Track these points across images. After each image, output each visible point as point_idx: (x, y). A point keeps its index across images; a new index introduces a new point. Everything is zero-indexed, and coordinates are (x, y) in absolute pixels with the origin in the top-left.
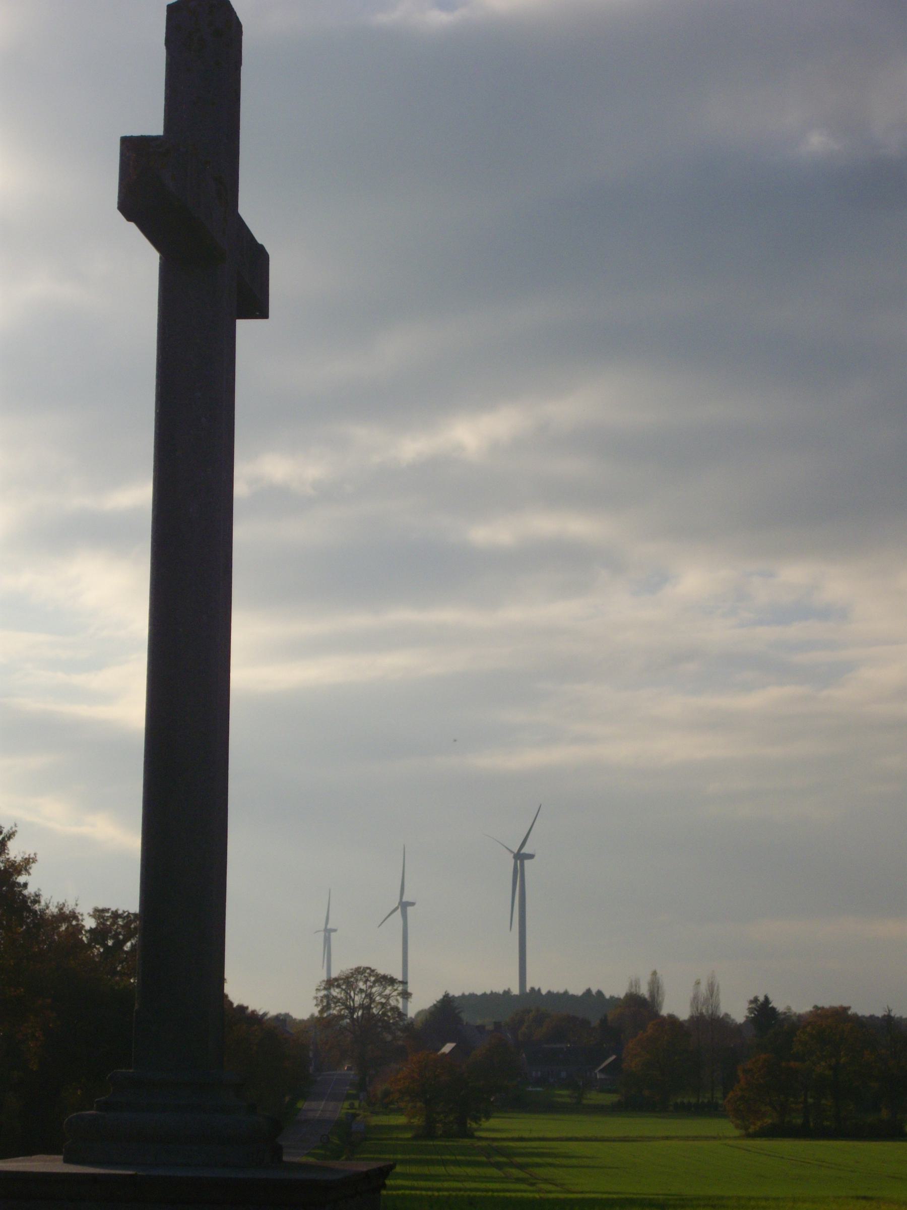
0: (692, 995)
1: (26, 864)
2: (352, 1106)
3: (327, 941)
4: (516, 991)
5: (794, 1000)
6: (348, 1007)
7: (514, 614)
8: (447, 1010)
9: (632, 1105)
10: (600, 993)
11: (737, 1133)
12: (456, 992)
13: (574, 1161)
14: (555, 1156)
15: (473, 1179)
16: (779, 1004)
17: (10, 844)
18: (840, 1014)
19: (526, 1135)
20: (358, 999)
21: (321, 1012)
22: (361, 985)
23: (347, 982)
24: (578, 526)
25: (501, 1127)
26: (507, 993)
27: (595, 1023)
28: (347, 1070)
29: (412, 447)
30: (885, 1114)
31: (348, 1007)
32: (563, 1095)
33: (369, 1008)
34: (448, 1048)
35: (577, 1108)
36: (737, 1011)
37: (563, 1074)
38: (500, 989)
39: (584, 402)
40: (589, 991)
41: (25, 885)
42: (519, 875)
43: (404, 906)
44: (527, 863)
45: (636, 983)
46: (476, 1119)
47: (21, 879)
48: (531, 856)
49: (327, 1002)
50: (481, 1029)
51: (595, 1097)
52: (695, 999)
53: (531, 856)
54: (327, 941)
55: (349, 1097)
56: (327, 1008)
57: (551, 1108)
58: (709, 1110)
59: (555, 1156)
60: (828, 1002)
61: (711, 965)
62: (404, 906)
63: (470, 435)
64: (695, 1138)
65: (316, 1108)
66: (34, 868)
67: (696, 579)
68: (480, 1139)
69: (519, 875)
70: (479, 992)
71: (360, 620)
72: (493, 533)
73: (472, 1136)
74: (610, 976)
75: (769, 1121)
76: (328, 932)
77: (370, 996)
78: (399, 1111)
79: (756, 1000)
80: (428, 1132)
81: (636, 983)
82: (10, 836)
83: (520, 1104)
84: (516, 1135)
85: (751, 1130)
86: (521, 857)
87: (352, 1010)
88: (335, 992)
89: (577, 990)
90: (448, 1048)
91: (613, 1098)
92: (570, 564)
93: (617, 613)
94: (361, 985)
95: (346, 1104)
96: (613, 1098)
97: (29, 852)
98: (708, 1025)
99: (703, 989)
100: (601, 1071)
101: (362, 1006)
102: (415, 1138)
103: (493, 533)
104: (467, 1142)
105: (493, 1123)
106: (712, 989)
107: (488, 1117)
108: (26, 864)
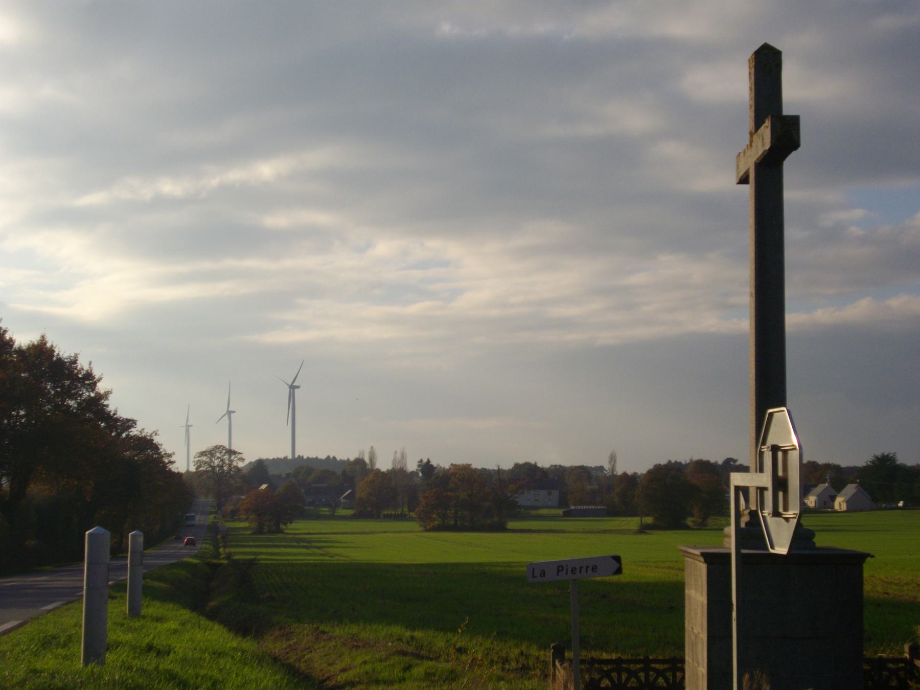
0: (392, 458)
1: (106, 395)
2: (215, 518)
3: (187, 431)
4: (290, 457)
5: (443, 461)
6: (211, 466)
7: (288, 263)
8: (260, 467)
9: (361, 515)
10: (334, 458)
11: (421, 529)
12: (264, 457)
13: (336, 545)
14: (337, 542)
15: (296, 555)
16: (434, 463)
17: (99, 385)
18: (467, 468)
19: (311, 531)
20: (216, 462)
21: (197, 468)
22: (218, 455)
23: (211, 453)
24: (321, 218)
25: (299, 527)
26: (285, 458)
27: (339, 472)
28: (211, 499)
29: (235, 175)
30: (496, 519)
31: (211, 466)
32: (325, 510)
33: (222, 467)
34: (264, 486)
35: (332, 517)
36: (412, 466)
37: (324, 500)
38: (282, 456)
39: (320, 156)
40: (329, 457)
41: (107, 406)
42: (292, 396)
43: (230, 413)
44: (296, 390)
45: (362, 453)
46: (285, 524)
47: (106, 403)
48: (298, 387)
49: (199, 464)
50: (279, 476)
51: (341, 512)
52: (394, 460)
53: (298, 387)
54: (187, 431)
55: (211, 513)
56: (200, 466)
57: (319, 517)
58: (401, 517)
59: (337, 542)
60: (460, 461)
61: (395, 442)
62: (230, 413)
63: (266, 170)
64: (399, 532)
65: (199, 519)
66: (111, 397)
67: (385, 247)
68: (288, 534)
69: (292, 396)
70: (271, 458)
71: (207, 265)
72: (278, 220)
73: (283, 533)
74: (344, 450)
75: (436, 523)
76: (188, 427)
77: (222, 460)
78: (240, 520)
79: (421, 461)
80: (259, 531)
81: (362, 453)
82: (99, 380)
83: (304, 516)
84: (306, 531)
85: (428, 527)
86: (293, 388)
87: (213, 468)
88: (204, 458)
89: (323, 456)
90: (264, 486)
91: (350, 512)
92: (320, 239)
93: (342, 263)
94: (218, 455)
95: (212, 517)
96: (350, 512)
97: (108, 388)
98: (398, 473)
99: (399, 455)
100: (345, 498)
101: (218, 466)
102: (254, 533)
103: (278, 220)
104: (280, 535)
105: (293, 526)
106: (403, 455)
107: (291, 523)
108: (106, 395)
